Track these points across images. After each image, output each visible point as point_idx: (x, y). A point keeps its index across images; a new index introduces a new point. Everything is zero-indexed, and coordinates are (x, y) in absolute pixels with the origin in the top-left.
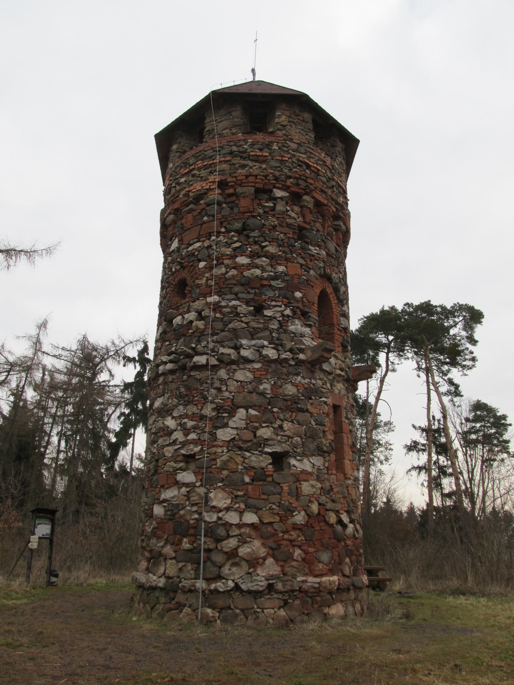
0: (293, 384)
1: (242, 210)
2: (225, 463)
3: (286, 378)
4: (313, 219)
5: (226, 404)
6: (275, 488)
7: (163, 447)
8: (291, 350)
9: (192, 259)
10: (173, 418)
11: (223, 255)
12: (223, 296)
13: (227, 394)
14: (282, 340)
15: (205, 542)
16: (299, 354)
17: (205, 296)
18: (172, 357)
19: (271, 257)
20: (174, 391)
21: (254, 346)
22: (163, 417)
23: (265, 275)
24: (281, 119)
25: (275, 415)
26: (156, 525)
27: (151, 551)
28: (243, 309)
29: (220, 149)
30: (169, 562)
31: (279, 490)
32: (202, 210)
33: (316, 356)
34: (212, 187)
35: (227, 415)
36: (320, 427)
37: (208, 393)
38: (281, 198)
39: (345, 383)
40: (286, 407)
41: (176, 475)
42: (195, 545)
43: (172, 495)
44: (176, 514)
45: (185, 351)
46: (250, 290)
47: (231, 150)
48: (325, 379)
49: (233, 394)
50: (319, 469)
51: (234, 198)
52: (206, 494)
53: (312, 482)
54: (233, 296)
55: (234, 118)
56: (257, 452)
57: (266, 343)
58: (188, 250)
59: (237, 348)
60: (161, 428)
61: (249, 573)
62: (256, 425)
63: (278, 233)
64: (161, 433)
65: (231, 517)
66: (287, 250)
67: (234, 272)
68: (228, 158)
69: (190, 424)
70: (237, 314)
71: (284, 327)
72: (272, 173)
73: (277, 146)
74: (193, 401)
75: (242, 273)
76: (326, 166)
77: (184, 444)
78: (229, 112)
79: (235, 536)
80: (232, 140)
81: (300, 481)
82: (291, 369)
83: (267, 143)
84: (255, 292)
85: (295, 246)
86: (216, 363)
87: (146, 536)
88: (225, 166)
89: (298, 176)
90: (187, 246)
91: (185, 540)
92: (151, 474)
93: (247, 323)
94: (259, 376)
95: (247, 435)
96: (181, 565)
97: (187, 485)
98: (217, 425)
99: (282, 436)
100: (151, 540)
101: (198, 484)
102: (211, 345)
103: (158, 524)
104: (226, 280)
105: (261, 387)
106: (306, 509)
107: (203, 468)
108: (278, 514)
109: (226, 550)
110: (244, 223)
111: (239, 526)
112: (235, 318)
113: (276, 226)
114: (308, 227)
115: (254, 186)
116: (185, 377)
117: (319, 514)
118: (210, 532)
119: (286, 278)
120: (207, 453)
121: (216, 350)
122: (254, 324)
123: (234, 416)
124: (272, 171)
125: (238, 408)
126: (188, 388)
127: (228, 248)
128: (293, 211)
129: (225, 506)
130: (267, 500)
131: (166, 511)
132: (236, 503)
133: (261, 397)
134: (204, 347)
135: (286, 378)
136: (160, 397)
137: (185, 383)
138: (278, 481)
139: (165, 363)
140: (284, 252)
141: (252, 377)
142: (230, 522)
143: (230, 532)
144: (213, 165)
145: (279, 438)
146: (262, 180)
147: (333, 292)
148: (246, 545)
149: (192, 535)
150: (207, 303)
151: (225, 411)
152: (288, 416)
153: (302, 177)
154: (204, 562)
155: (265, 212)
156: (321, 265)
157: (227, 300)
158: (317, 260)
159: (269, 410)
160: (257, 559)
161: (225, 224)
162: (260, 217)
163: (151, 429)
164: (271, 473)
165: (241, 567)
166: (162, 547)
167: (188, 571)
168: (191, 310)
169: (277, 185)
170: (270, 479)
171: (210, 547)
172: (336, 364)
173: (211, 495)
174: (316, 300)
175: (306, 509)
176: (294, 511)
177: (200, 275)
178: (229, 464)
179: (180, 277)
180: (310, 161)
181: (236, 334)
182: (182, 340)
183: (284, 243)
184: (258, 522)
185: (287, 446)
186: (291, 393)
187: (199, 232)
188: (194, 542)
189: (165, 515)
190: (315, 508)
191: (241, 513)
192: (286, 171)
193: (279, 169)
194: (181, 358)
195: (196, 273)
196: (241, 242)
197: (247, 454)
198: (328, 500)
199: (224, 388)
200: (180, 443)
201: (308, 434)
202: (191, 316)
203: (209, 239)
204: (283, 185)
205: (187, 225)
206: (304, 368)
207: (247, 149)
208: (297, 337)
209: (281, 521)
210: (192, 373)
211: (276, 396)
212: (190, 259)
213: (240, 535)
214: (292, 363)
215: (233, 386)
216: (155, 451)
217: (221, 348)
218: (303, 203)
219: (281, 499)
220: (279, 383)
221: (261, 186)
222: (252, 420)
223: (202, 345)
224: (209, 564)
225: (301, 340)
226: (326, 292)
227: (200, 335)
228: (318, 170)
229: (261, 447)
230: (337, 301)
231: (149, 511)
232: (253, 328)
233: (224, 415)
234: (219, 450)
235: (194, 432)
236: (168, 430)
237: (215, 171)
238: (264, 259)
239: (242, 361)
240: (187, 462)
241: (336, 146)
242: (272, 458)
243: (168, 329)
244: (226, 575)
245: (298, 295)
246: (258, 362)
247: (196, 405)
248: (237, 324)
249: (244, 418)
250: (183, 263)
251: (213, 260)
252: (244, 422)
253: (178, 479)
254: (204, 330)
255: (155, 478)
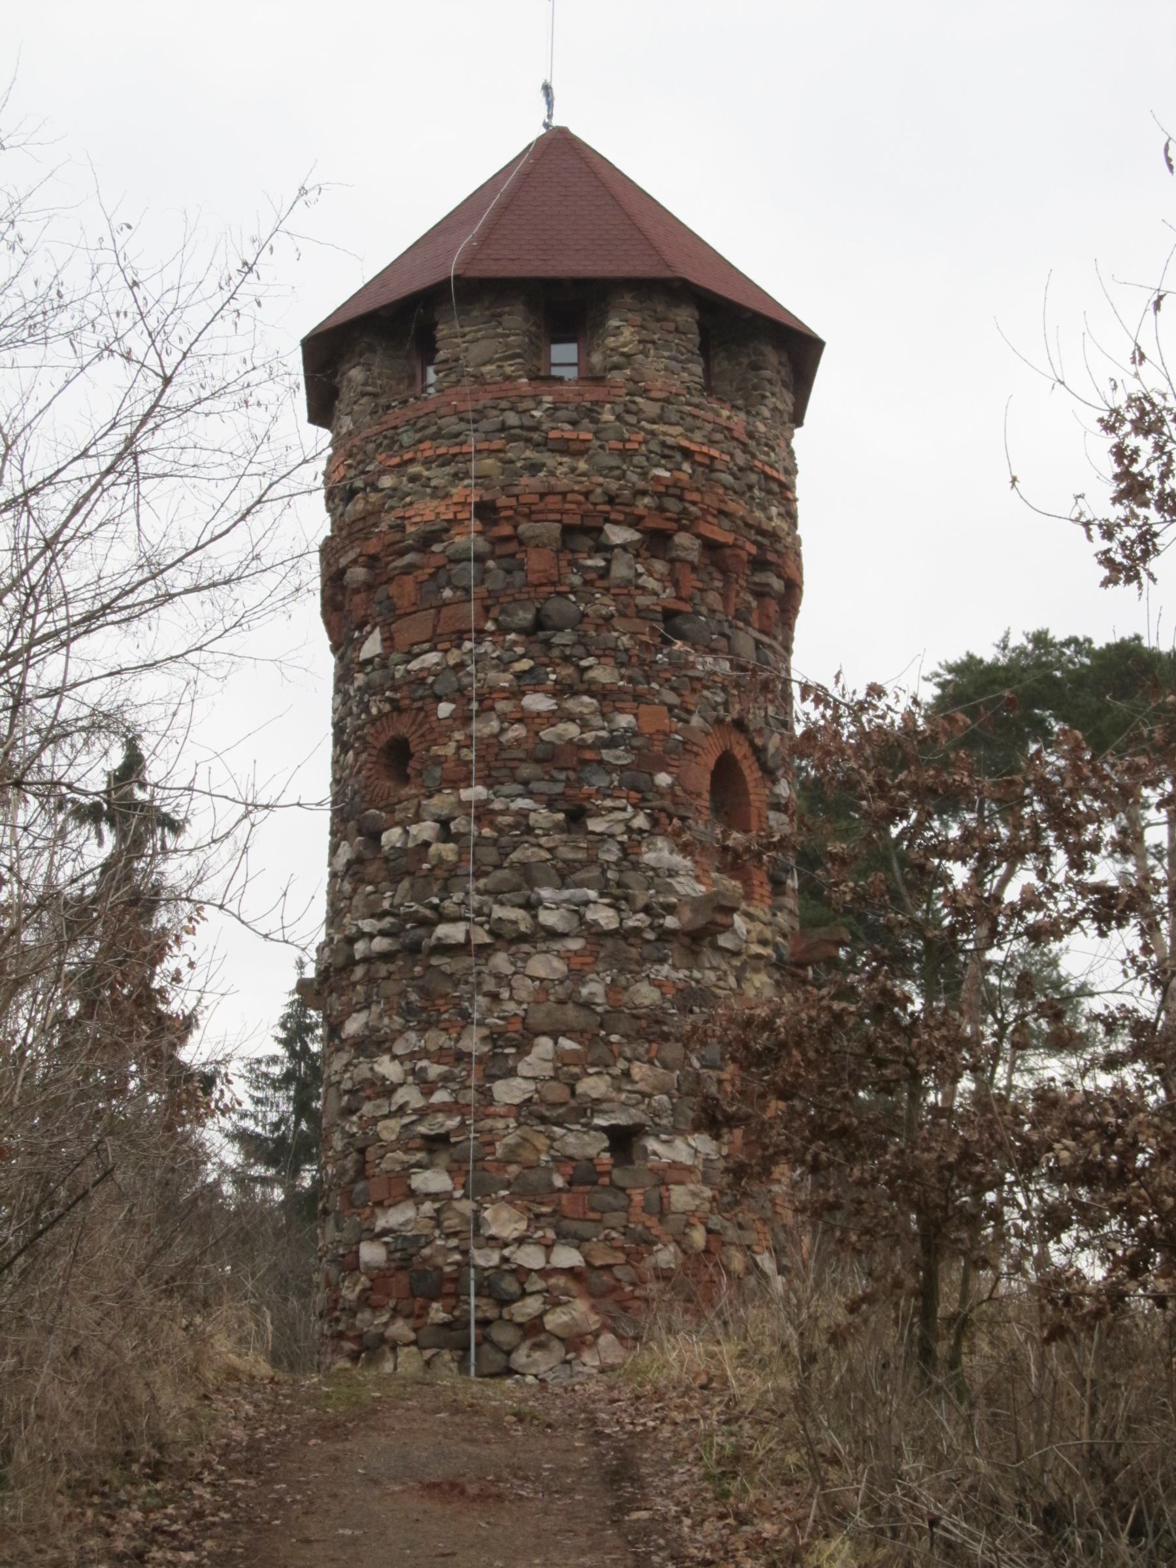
0: (653, 983)
1: (533, 578)
2: (512, 1150)
3: (637, 968)
4: (700, 585)
5: (511, 1028)
6: (616, 1197)
7: (375, 1120)
8: (647, 909)
9: (420, 692)
10: (394, 1057)
11: (492, 689)
12: (497, 787)
13: (511, 1007)
14: (628, 887)
15: (477, 1307)
16: (664, 917)
17: (455, 784)
18: (387, 922)
19: (603, 694)
20: (395, 999)
21: (567, 901)
22: (371, 1056)
23: (589, 737)
24: (622, 339)
25: (616, 1049)
26: (368, 1284)
27: (359, 1337)
28: (542, 817)
29: (477, 416)
30: (403, 1352)
31: (625, 1203)
32: (438, 568)
33: (701, 921)
34: (460, 516)
35: (512, 1050)
36: (711, 1073)
37: (472, 1005)
38: (624, 547)
39: (774, 971)
40: (638, 1032)
41: (409, 1177)
42: (457, 1313)
43: (402, 1219)
44: (413, 1255)
45: (417, 912)
46: (555, 774)
47: (503, 422)
48: (724, 966)
49: (525, 1006)
50: (707, 1161)
51: (512, 547)
52: (476, 1213)
53: (691, 1187)
54: (519, 788)
55: (508, 336)
56: (578, 1127)
57: (592, 894)
58: (410, 667)
59: (531, 906)
60: (366, 1080)
61: (567, 1362)
62: (575, 1070)
63: (615, 634)
64: (368, 1092)
65: (528, 1255)
66: (637, 672)
67: (517, 731)
68: (497, 444)
69: (435, 1071)
70: (529, 830)
71: (632, 857)
72: (601, 485)
73: (613, 412)
74: (438, 1021)
75: (537, 733)
76: (734, 439)
77: (423, 1114)
78: (493, 316)
79: (538, 1292)
80: (502, 394)
81: (667, 1184)
82: (647, 950)
83: (588, 405)
84: (568, 778)
85: (656, 662)
86: (487, 940)
87: (343, 1310)
88: (489, 463)
89: (662, 489)
90: (405, 657)
91: (435, 1305)
92: (346, 1179)
93: (550, 850)
94: (578, 967)
95: (557, 1092)
96: (428, 1353)
97: (434, 1197)
98: (495, 1071)
99: (630, 1092)
100: (359, 1316)
101: (458, 1193)
102: (475, 900)
103: (372, 1280)
104: (502, 747)
105: (585, 991)
106: (680, 1240)
107: (466, 1161)
108: (622, 1249)
109: (519, 1319)
110: (538, 610)
111: (544, 1273)
112: (526, 838)
113: (612, 616)
114: (686, 607)
115: (559, 521)
116: (418, 969)
117: (707, 1251)
118: (487, 1288)
119: (637, 742)
120: (476, 1131)
121: (486, 910)
122: (566, 853)
123: (528, 1053)
124: (601, 480)
125: (537, 1035)
126: (424, 992)
127: (504, 671)
128: (650, 573)
129: (515, 1234)
130: (600, 1221)
131: (390, 1252)
132: (537, 1229)
133: (584, 1012)
134: (459, 904)
135: (637, 968)
136: (358, 1011)
137: (420, 982)
138: (621, 1184)
139: (371, 936)
140: (630, 680)
141: (565, 969)
142: (526, 1265)
143: (526, 1286)
144: (460, 458)
145: (623, 1096)
146: (579, 503)
147: (749, 754)
148: (559, 1310)
149: (449, 1295)
150: (460, 802)
151: (510, 1043)
152: (641, 1050)
153: (672, 491)
154: (478, 1345)
155: (586, 583)
156: (719, 699)
157: (507, 797)
158: (707, 688)
159: (602, 1039)
160: (581, 1335)
161: (494, 612)
162: (574, 593)
163: (339, 1083)
164: (609, 1168)
165: (550, 1351)
166: (386, 1325)
167: (445, 1365)
168: (424, 815)
169: (613, 516)
170: (605, 1180)
171: (488, 1314)
172: (749, 932)
173: (487, 1214)
174: (706, 783)
175: (680, 1240)
176: (655, 1243)
177: (442, 734)
178: (521, 1151)
179: (392, 733)
180: (691, 441)
181: (528, 875)
182: (405, 884)
183: (630, 657)
184: (583, 1264)
185: (639, 1113)
186: (647, 1002)
187: (435, 627)
188: (454, 1308)
189: (389, 1260)
190: (698, 1237)
191: (549, 1248)
192: (634, 478)
193: (617, 473)
194: (408, 926)
195: (432, 729)
196: (532, 658)
197: (558, 1131)
198: (727, 1224)
199: (505, 994)
200: (415, 1111)
201: (684, 1088)
202: (425, 830)
203: (459, 647)
204: (626, 514)
205: (404, 604)
206: (675, 945)
207: (540, 422)
208: (660, 877)
209: (627, 1263)
210: (434, 961)
211: (615, 1010)
212: (415, 691)
213: (547, 1291)
214: (650, 936)
215: (524, 988)
216: (355, 1129)
217: (496, 907)
218: (674, 554)
219: (628, 1221)
220: (622, 981)
221: (575, 520)
222: (566, 1061)
223: (455, 899)
224: (486, 1347)
225: (670, 884)
226: (733, 757)
227: (449, 877)
228: (713, 458)
229: (584, 1115)
230: (760, 774)
231: (349, 1258)
232: (565, 861)
233: (507, 1051)
234: (500, 1124)
235: (444, 1087)
236: (383, 1084)
237: (467, 475)
238: (586, 699)
239: (543, 934)
240: (431, 1151)
241: (761, 368)
242: (610, 1138)
243: (368, 854)
244: (523, 1366)
245: (663, 779)
246: (577, 936)
247: (446, 1030)
248: (529, 853)
249: (550, 1056)
250: (397, 701)
251: (470, 700)
252: (550, 1065)
253: (413, 1186)
254: (456, 865)
255: (360, 1186)
